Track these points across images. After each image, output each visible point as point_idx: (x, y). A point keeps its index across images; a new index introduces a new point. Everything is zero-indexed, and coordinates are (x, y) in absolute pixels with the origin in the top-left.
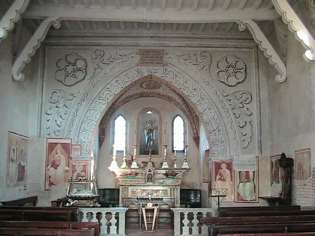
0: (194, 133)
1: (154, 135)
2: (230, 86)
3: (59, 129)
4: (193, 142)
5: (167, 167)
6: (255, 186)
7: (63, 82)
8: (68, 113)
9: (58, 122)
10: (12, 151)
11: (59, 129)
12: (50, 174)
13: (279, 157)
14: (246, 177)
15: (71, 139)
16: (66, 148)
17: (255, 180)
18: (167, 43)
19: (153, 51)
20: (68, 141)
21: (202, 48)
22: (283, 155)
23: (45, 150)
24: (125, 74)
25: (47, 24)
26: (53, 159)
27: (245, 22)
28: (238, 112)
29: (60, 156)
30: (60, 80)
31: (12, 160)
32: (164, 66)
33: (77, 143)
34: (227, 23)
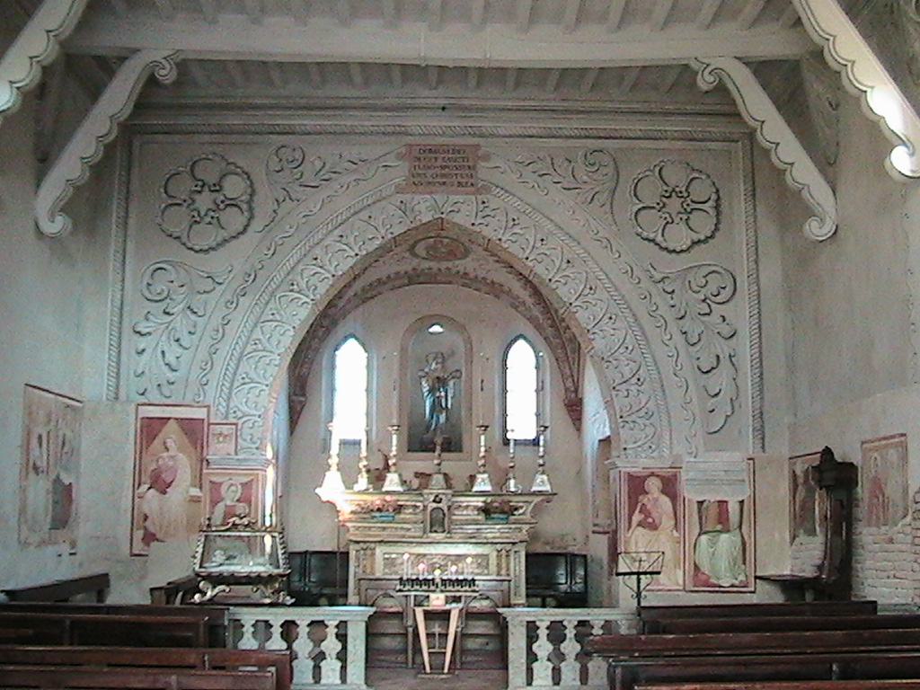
0: (567, 390)
1: (449, 395)
2: (671, 252)
3: (171, 376)
4: (562, 414)
5: (488, 488)
6: (744, 544)
7: (184, 239)
8: (199, 330)
9: (170, 358)
10: (34, 442)
11: (171, 376)
12: (146, 509)
13: (816, 460)
14: (718, 518)
15: (208, 407)
16: (194, 432)
17: (744, 527)
18: (487, 125)
19: (446, 149)
20: (199, 413)
21: (589, 141)
22: (827, 452)
23: (132, 438)
24: (364, 215)
25: (139, 70)
26: (154, 466)
27: (715, 63)
28: (694, 328)
29: (176, 458)
30: (175, 235)
31: (36, 468)
32: (478, 192)
33: (226, 418)
34: (663, 69)
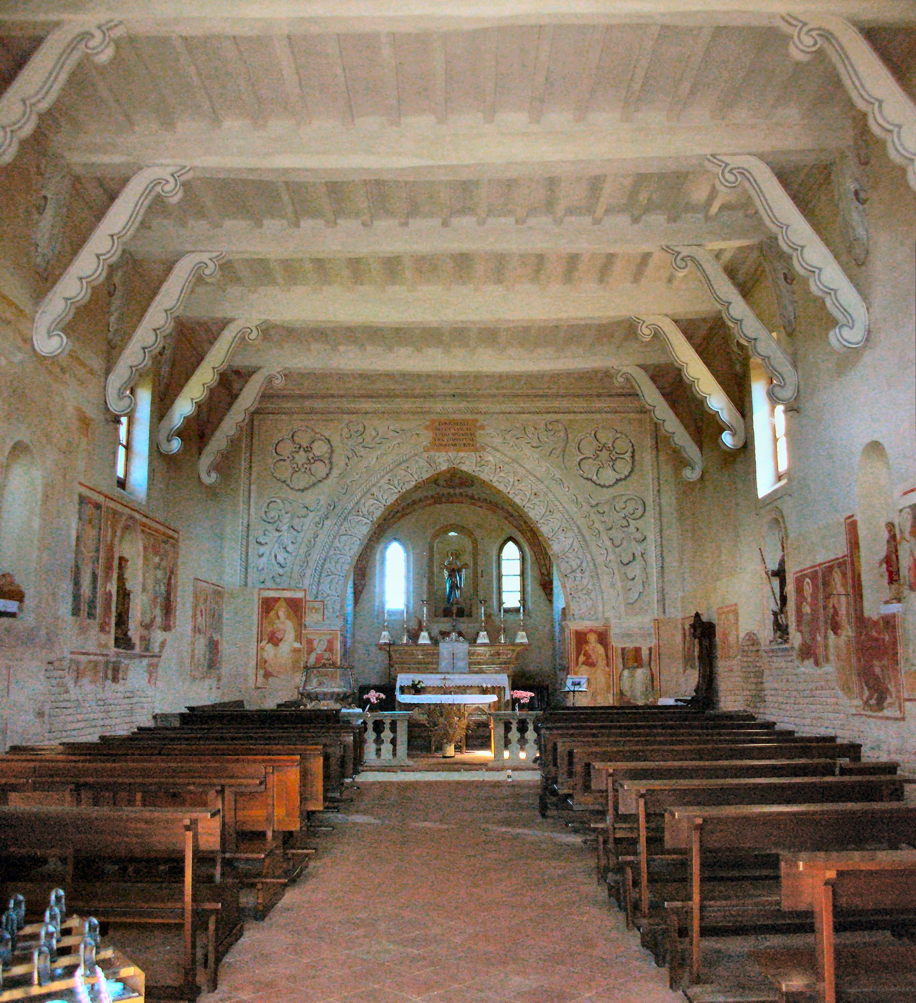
0: (542, 574)
1: (463, 579)
2: (603, 486)
3: (281, 571)
4: (540, 592)
5: (487, 641)
6: (652, 675)
7: (288, 482)
8: (299, 540)
9: (280, 559)
10: (198, 613)
11: (281, 571)
12: (265, 655)
13: (692, 621)
14: (633, 658)
15: (305, 590)
16: (296, 607)
17: (653, 664)
18: (482, 406)
19: (456, 422)
20: (299, 595)
21: (550, 415)
22: (697, 615)
23: (256, 609)
24: (403, 466)
25: (262, 380)
26: (270, 629)
27: (625, 370)
28: (618, 535)
29: (286, 625)
30: (283, 479)
31: (199, 631)
32: (476, 450)
33: (316, 597)
34: (596, 372)
